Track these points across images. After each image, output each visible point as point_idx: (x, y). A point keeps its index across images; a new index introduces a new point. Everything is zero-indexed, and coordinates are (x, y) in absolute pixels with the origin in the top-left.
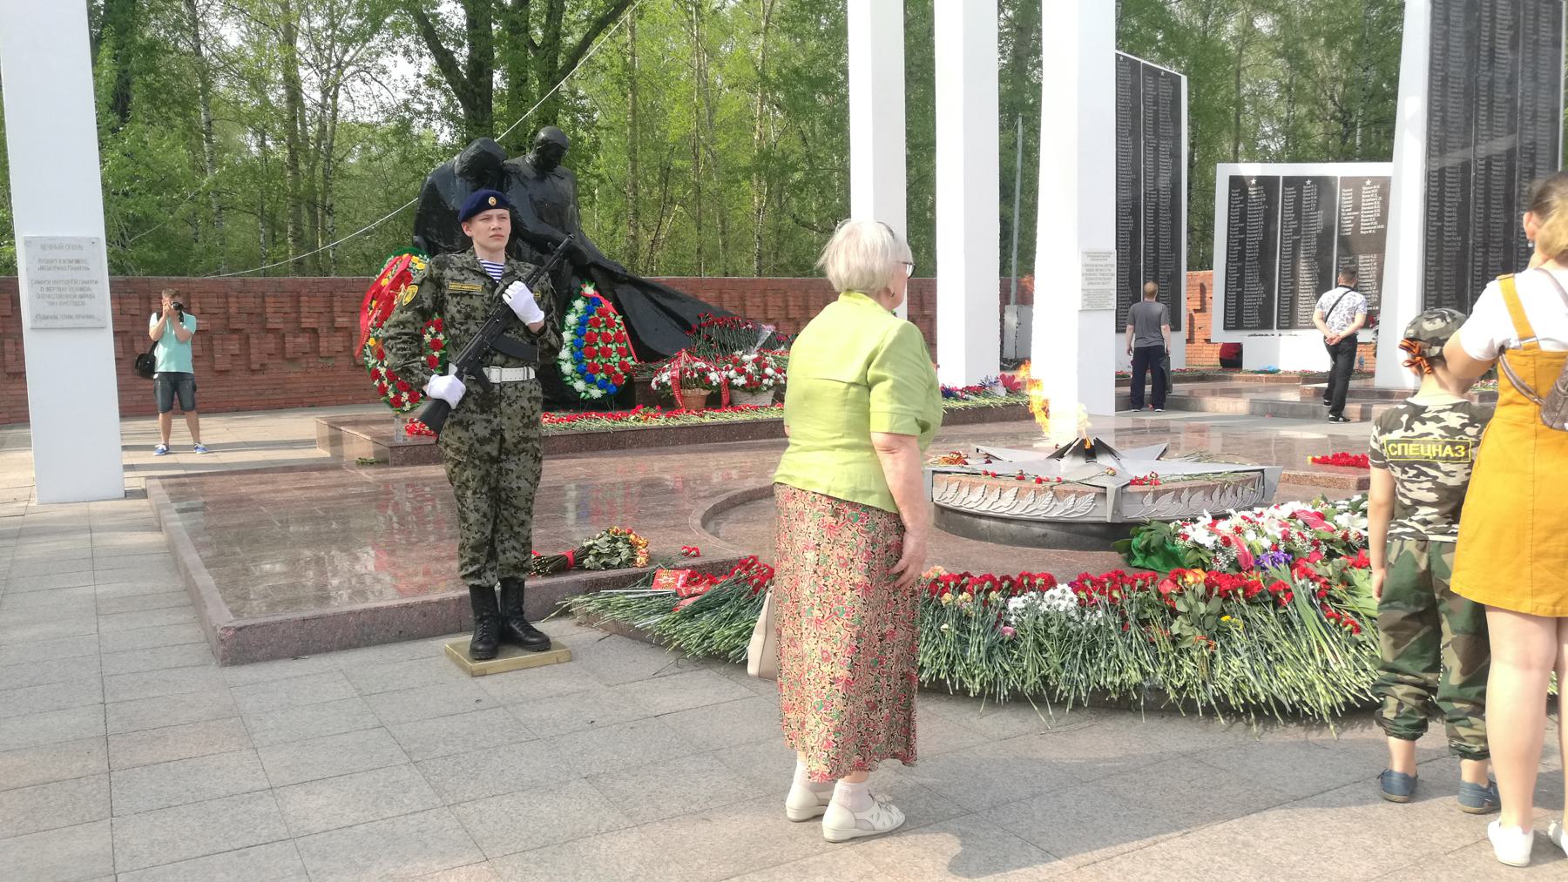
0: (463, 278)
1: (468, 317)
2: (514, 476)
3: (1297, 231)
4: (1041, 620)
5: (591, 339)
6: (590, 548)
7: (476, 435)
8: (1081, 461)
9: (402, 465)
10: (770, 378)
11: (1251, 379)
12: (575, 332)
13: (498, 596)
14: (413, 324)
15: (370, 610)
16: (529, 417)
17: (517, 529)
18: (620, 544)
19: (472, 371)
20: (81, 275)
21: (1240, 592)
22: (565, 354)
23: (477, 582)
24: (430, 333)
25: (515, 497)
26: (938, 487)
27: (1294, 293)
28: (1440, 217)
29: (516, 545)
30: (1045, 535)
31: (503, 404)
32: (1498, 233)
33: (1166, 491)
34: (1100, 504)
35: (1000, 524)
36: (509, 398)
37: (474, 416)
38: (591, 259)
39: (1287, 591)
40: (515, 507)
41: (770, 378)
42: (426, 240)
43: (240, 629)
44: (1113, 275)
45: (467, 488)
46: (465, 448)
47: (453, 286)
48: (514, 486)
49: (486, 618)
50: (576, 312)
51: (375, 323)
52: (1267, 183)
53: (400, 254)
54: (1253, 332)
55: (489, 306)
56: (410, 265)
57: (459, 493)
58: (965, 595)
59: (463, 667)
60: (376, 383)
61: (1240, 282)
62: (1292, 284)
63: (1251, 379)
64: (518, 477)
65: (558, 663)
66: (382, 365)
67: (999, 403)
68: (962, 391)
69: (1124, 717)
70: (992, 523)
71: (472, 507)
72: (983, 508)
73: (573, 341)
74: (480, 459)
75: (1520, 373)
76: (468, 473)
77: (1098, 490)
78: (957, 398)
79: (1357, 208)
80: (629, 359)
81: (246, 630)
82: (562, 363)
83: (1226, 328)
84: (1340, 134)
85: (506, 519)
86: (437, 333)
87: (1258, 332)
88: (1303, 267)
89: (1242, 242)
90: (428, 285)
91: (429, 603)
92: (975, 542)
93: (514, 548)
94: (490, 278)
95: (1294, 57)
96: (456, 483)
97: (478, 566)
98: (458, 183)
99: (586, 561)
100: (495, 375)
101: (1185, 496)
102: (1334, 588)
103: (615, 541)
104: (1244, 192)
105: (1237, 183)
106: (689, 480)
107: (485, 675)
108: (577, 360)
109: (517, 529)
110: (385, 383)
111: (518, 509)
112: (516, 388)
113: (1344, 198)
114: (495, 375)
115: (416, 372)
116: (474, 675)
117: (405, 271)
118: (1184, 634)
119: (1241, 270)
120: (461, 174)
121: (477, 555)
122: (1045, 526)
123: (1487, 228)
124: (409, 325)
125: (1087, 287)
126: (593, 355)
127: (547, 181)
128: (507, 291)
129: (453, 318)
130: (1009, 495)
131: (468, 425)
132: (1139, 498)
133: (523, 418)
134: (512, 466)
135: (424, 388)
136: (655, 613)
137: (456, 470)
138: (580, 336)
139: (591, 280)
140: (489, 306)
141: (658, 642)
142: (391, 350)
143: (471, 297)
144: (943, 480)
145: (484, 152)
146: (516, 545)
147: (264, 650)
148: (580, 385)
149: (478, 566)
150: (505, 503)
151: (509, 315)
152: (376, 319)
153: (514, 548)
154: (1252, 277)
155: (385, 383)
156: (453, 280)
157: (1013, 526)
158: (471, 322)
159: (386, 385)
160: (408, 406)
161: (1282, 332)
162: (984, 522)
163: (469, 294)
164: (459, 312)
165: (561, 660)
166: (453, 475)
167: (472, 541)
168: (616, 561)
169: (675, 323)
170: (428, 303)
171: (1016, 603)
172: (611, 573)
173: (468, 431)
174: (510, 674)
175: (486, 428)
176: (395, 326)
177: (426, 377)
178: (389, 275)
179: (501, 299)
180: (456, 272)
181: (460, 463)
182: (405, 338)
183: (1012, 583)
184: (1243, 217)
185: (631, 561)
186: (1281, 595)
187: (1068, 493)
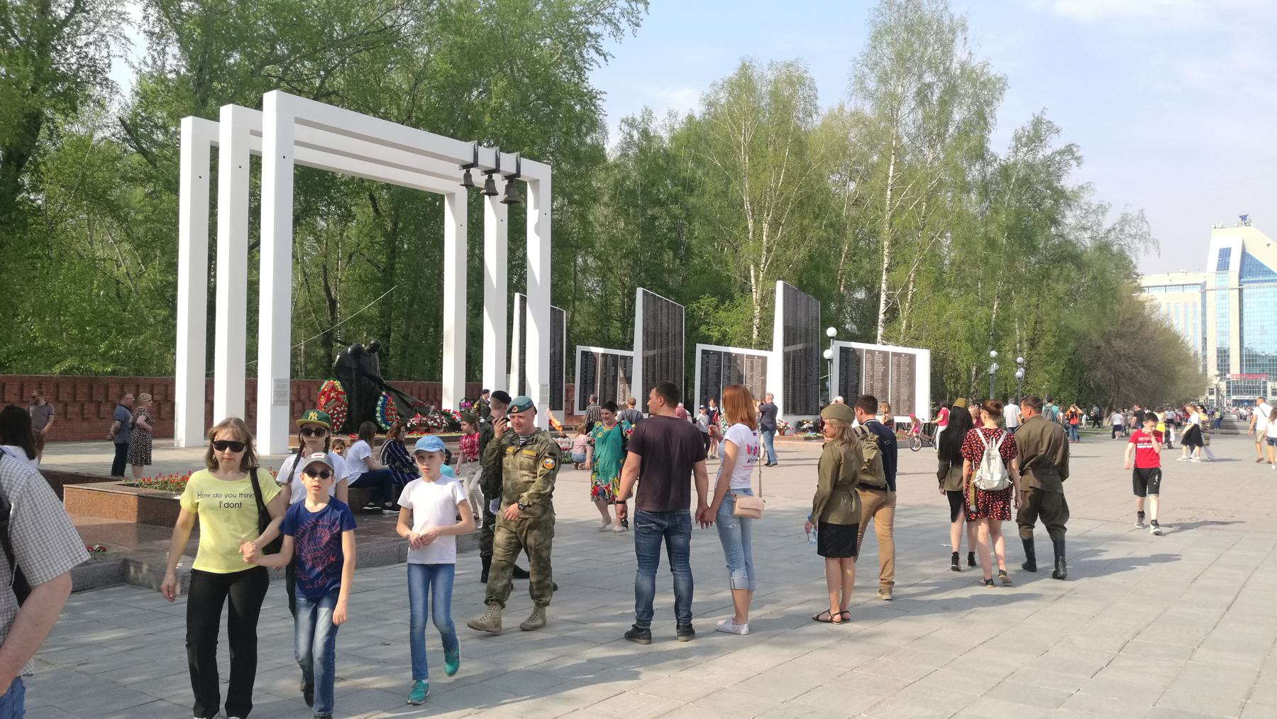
3: (605, 374)
5: (387, 410)
80: (219, 87)
89: (586, 377)
106: (490, 591)
108: (382, 416)
119: (585, 387)
126: (388, 415)
148: (383, 425)
169: (677, 661)
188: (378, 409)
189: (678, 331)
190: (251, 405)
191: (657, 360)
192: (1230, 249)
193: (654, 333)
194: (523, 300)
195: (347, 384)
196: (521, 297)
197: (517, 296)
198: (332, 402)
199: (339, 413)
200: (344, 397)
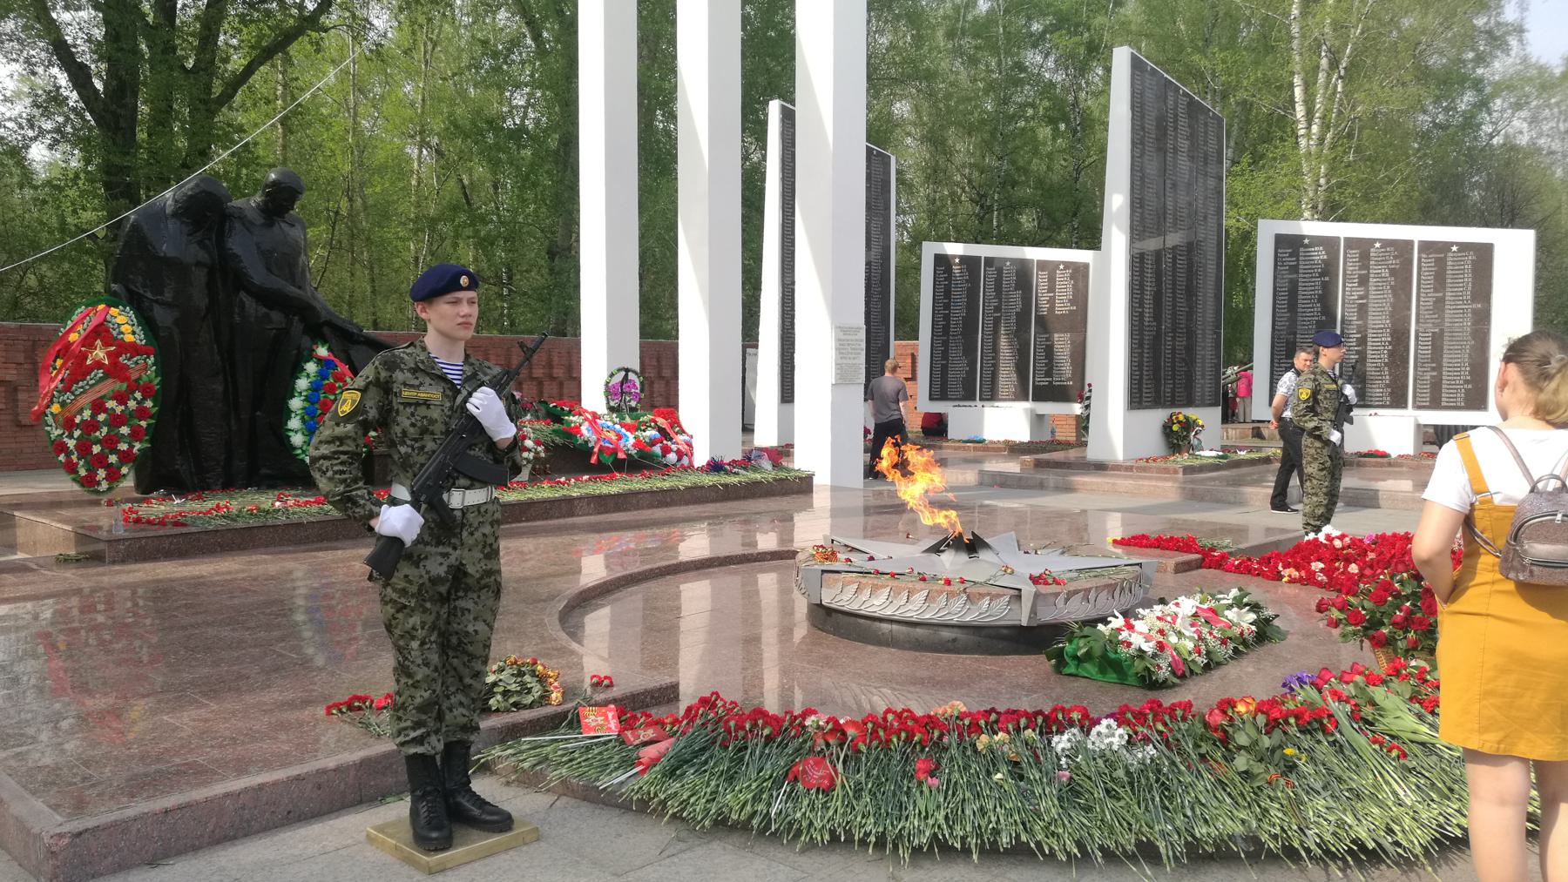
0: (416, 382)
1: (424, 431)
2: (471, 617)
3: (997, 309)
4: (1100, 762)
6: (495, 684)
7: (428, 572)
8: (963, 557)
9: (123, 561)
10: (529, 450)
11: (959, 448)
12: (307, 399)
14: (355, 440)
15: (253, 789)
16: (491, 545)
17: (468, 681)
18: (527, 678)
19: (428, 500)
21: (1292, 720)
23: (420, 750)
24: (135, 399)
25: (471, 643)
26: (829, 587)
27: (995, 366)
28: (1141, 304)
29: (463, 699)
30: (954, 640)
31: (465, 534)
32: (1182, 319)
33: (1076, 592)
34: (1015, 606)
35: (904, 629)
36: (471, 526)
37: (428, 548)
38: (324, 316)
39: (1330, 716)
40: (469, 655)
41: (529, 450)
42: (129, 290)
43: (80, 834)
45: (413, 638)
46: (413, 589)
47: (406, 393)
48: (470, 629)
49: (430, 793)
50: (308, 376)
51: (60, 386)
52: (970, 262)
53: (94, 304)
54: (957, 403)
55: (450, 417)
56: (108, 317)
57: (401, 643)
58: (1001, 735)
59: (409, 861)
60: (62, 458)
61: (945, 355)
62: (994, 358)
63: (959, 448)
64: (475, 619)
65: (525, 844)
66: (71, 436)
67: (770, 477)
68: (729, 464)
69: (1223, 871)
70: (895, 627)
71: (419, 661)
72: (888, 612)
73: (304, 408)
74: (431, 600)
75: (443, 325)
76: (415, 620)
77: (1012, 592)
78: (727, 473)
79: (1052, 289)
81: (87, 835)
82: (291, 434)
83: (931, 398)
84: (978, 215)
85: (455, 669)
86: (144, 399)
87: (961, 403)
88: (1003, 342)
89: (947, 318)
90: (373, 391)
91: (324, 772)
92: (875, 648)
93: (461, 704)
94: (450, 382)
95: (935, 140)
96: (398, 632)
97: (423, 730)
98: (170, 226)
99: (492, 702)
100: (458, 499)
101: (1092, 596)
102: (1363, 709)
103: (521, 674)
104: (949, 270)
105: (942, 261)
107: (443, 870)
109: (468, 681)
110: (74, 458)
111: (472, 657)
112: (479, 511)
113: (1039, 281)
114: (458, 499)
115: (362, 502)
116: (431, 872)
117: (101, 324)
118: (1256, 771)
119: (945, 344)
120: (175, 214)
121: (424, 717)
122: (955, 630)
123: (1174, 314)
124: (349, 442)
125: (840, 361)
127: (276, 229)
128: (471, 400)
129: (404, 433)
130: (920, 597)
131: (420, 559)
132: (1052, 599)
133: (484, 547)
134: (469, 604)
135: (372, 523)
136: (616, 769)
137: (400, 616)
138: (313, 404)
139: (324, 341)
140: (450, 417)
141: (642, 807)
142: (324, 473)
143: (428, 407)
144: (837, 581)
145: (204, 191)
146: (463, 699)
147: (110, 859)
149: (423, 730)
150: (455, 649)
151: (474, 426)
152: (62, 381)
153: (461, 704)
154: (956, 353)
155: (74, 458)
156: (405, 384)
157: (919, 630)
158: (427, 437)
159: (75, 460)
160: (104, 486)
161: (985, 403)
162: (886, 627)
163: (426, 404)
164: (413, 425)
165: (527, 841)
166: (394, 622)
167: (418, 700)
168: (528, 700)
170: (373, 413)
171: (1061, 742)
172: (526, 715)
173: (418, 567)
174: (476, 865)
175: (441, 564)
176: (328, 442)
177: (375, 509)
178: (80, 328)
179: (463, 408)
180: (408, 375)
181: (405, 607)
182: (343, 457)
183: (1046, 718)
184: (947, 293)
185: (544, 699)
186: (1325, 721)
187: (982, 596)
188: (296, 403)
190: (659, 387)
191: (1166, 265)
193: (1206, 164)
194: (788, 118)
195: (163, 317)
196: (783, 108)
197: (774, 108)
198: (89, 380)
199: (116, 421)
200: (146, 369)
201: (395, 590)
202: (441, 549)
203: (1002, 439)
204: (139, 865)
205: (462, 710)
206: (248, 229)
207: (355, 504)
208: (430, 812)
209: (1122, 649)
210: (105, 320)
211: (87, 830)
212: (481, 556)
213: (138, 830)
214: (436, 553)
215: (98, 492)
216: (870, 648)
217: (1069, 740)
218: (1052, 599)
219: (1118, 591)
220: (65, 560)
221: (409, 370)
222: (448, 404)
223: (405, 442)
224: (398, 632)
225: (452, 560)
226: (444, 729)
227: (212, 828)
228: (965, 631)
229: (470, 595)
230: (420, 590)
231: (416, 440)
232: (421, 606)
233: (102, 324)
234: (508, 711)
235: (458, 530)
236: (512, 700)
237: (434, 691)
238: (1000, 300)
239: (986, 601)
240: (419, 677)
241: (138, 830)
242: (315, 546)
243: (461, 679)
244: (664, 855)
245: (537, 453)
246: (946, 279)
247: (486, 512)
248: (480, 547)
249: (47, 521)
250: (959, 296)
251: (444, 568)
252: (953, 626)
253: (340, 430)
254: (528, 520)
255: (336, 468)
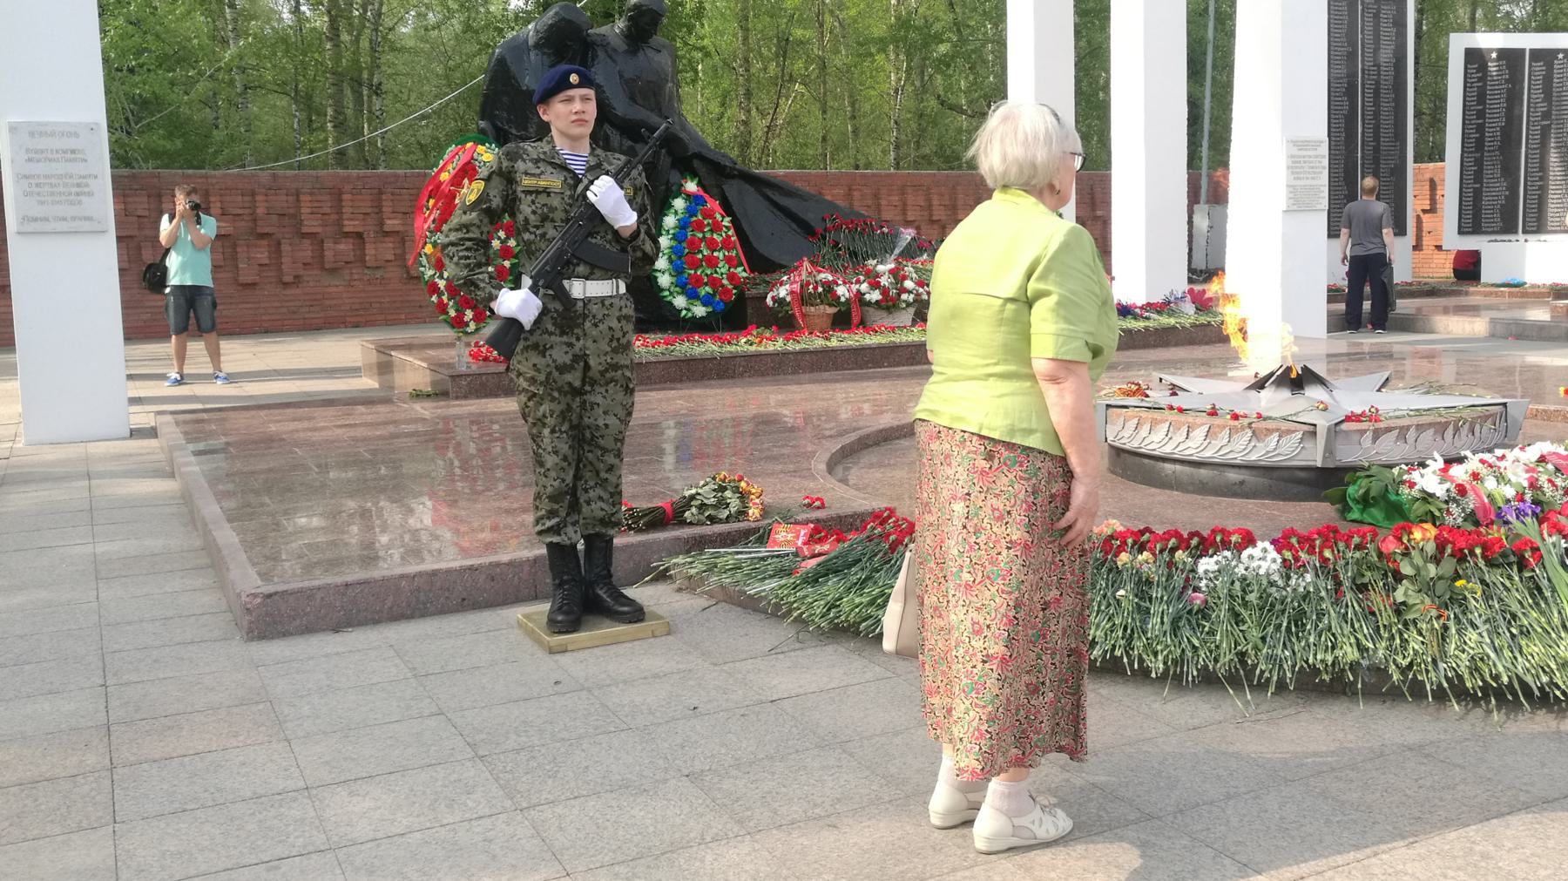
0: (538, 171)
1: (544, 218)
5: (694, 246)
7: (554, 361)
8: (1286, 393)
9: (465, 397)
10: (910, 292)
11: (1491, 294)
13: (581, 556)
14: (479, 227)
16: (618, 340)
17: (603, 475)
18: (728, 494)
19: (550, 284)
20: (78, 169)
22: (662, 263)
23: (556, 539)
24: (499, 238)
25: (602, 437)
29: (602, 494)
30: (1242, 483)
31: (588, 324)
34: (1308, 444)
36: (594, 317)
39: (1536, 550)
40: (602, 449)
41: (910, 292)
43: (270, 596)
44: (1324, 168)
45: (544, 425)
46: (542, 377)
47: (527, 182)
48: (601, 422)
49: (566, 582)
51: (432, 226)
52: (1511, 57)
53: (464, 143)
54: (1493, 237)
55: (571, 205)
56: (475, 155)
57: (534, 431)
61: (1478, 177)
62: (1541, 179)
63: (1491, 294)
64: (605, 413)
65: (654, 636)
66: (441, 277)
67: (1187, 322)
68: (1142, 308)
70: (1178, 467)
71: (550, 449)
72: (1167, 450)
73: (671, 248)
77: (1306, 428)
78: (1136, 317)
81: (276, 597)
82: (658, 274)
83: (1461, 232)
85: (590, 463)
86: (508, 238)
87: (1499, 237)
89: (1481, 128)
90: (496, 180)
91: (498, 564)
93: (600, 498)
100: (579, 289)
101: (1411, 434)
103: (722, 489)
104: (1483, 67)
105: (1474, 57)
108: (677, 271)
109: (603, 475)
110: (445, 298)
112: (603, 305)
114: (579, 289)
115: (482, 285)
116: (552, 651)
119: (1479, 163)
120: (537, 46)
122: (1243, 471)
126: (696, 265)
127: (641, 54)
128: (592, 187)
129: (526, 220)
130: (1199, 434)
132: (1356, 437)
133: (611, 340)
134: (599, 399)
136: (771, 577)
137: (531, 404)
138: (680, 242)
139: (694, 174)
140: (571, 205)
141: (775, 611)
142: (451, 258)
143: (549, 194)
144: (1119, 416)
146: (602, 494)
147: (298, 621)
148: (680, 301)
152: (434, 221)
153: (600, 498)
154: (1492, 171)
155: (445, 298)
156: (526, 174)
157: (1203, 472)
158: (548, 225)
159: (445, 300)
160: (472, 326)
161: (1529, 237)
162: (1169, 467)
163: (546, 192)
164: (534, 212)
165: (657, 633)
168: (724, 514)
170: (496, 202)
171: (1207, 564)
172: (718, 528)
173: (544, 356)
174: (595, 650)
176: (457, 230)
178: (450, 167)
179: (585, 197)
180: (530, 164)
181: (535, 395)
182: (468, 244)
183: (1203, 540)
184: (1482, 97)
185: (742, 513)
187: (1270, 431)
189: (1386, 55)
192: (13, 129)
201: (525, 379)
202: (565, 339)
203: (1549, 283)
204: (324, 630)
205: (600, 504)
206: (610, 57)
207: (477, 287)
208: (564, 599)
209: (1404, 490)
210: (472, 158)
211: (276, 593)
212: (609, 349)
213: (322, 598)
214: (561, 342)
215: (467, 333)
216: (1153, 490)
217: (1216, 563)
218: (1356, 437)
219: (1450, 431)
220: (417, 395)
221: (531, 160)
222: (568, 193)
223: (528, 230)
224: (530, 420)
225: (577, 350)
226: (581, 521)
227: (389, 604)
228: (1254, 473)
229: (598, 389)
230: (547, 379)
231: (537, 227)
232: (550, 395)
233: (469, 162)
234: (703, 524)
235: (580, 321)
236: (707, 514)
237: (563, 481)
238: (1550, 105)
239: (1275, 437)
240: (548, 465)
241: (322, 598)
242: (657, 386)
243: (598, 473)
244: (773, 652)
245: (918, 295)
246: (1480, 79)
247: (611, 305)
248: (607, 340)
249: (411, 359)
250: (1496, 105)
251: (570, 356)
252: (1239, 467)
253: (466, 218)
254: (890, 366)
255: (461, 254)
